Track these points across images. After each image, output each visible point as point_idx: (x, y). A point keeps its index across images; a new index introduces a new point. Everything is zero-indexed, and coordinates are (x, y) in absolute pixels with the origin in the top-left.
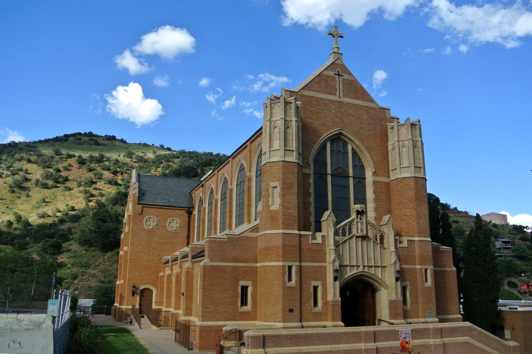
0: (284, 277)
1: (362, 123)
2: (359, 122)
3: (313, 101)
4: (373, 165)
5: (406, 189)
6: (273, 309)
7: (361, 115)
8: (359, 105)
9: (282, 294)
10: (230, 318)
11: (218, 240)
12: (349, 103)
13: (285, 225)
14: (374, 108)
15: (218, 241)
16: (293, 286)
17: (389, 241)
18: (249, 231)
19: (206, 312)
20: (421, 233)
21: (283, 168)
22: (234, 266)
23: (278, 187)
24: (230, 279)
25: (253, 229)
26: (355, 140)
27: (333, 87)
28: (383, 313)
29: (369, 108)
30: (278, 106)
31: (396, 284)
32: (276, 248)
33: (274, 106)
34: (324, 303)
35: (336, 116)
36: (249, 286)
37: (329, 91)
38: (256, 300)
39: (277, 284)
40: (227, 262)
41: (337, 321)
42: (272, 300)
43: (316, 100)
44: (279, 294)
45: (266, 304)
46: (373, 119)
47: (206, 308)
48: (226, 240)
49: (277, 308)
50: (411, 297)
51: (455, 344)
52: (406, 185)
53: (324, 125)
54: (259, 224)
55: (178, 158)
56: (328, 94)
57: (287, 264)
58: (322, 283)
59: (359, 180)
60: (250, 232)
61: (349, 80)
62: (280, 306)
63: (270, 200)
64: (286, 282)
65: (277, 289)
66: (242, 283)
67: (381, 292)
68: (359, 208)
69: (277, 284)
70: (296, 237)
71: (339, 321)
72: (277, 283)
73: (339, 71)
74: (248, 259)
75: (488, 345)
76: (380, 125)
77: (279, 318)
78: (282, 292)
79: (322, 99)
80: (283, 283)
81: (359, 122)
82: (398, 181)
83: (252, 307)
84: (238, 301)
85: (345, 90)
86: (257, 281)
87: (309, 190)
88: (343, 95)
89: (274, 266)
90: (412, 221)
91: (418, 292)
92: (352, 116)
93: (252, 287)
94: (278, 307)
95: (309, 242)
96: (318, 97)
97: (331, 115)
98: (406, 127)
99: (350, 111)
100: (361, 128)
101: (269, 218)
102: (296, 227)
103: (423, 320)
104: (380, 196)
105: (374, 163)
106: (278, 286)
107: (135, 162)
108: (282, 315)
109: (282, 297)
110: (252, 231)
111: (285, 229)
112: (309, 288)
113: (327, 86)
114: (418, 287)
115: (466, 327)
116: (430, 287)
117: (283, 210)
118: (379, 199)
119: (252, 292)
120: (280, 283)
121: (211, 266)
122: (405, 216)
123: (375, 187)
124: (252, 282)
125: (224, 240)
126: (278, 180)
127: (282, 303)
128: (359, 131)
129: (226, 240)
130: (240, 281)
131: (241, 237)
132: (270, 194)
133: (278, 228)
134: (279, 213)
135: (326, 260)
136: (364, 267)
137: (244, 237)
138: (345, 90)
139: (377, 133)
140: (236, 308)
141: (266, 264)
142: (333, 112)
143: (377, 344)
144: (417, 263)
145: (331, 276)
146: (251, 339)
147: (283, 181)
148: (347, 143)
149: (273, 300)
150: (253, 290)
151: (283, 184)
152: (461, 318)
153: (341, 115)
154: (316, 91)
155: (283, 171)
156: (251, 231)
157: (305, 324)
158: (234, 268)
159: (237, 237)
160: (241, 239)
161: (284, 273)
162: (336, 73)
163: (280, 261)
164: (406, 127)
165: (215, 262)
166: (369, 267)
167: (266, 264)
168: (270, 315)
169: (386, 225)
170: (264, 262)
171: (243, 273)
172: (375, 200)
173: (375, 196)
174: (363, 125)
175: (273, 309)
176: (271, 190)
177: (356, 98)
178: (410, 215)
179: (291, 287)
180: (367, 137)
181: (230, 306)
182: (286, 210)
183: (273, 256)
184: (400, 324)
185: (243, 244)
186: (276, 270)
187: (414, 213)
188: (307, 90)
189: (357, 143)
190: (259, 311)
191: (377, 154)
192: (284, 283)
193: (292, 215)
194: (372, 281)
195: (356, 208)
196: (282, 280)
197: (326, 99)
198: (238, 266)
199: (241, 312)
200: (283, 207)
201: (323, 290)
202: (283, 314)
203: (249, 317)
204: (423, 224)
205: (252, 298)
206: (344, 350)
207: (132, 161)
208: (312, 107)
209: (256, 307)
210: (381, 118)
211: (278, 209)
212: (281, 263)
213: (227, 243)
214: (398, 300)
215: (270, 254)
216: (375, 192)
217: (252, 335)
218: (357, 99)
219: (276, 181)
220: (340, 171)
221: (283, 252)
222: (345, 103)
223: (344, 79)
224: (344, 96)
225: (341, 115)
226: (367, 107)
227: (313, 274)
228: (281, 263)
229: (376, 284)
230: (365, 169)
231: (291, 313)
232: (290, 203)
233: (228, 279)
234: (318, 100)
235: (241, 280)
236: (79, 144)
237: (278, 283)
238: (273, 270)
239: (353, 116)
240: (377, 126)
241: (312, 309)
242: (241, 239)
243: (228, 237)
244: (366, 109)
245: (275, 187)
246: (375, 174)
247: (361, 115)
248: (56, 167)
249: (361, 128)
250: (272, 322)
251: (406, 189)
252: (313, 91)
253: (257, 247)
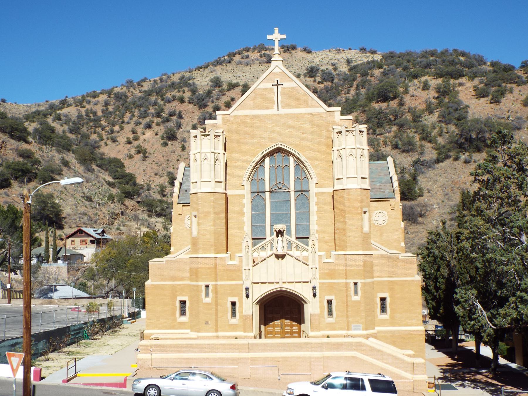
1: (303, 133)
5: (340, 202)
7: (302, 124)
11: (157, 263)
12: (289, 114)
16: (209, 302)
19: (150, 323)
20: (351, 247)
22: (172, 285)
27: (271, 100)
35: (274, 131)
37: (266, 106)
41: (248, 333)
43: (250, 118)
46: (317, 126)
47: (149, 319)
51: (265, 359)
52: (339, 197)
53: (260, 143)
55: (380, 67)
56: (264, 109)
58: (239, 299)
60: (185, 254)
61: (290, 88)
68: (281, 228)
73: (277, 81)
75: (382, 360)
76: (326, 132)
79: (258, 116)
81: (301, 132)
85: (284, 100)
87: (243, 211)
88: (282, 106)
92: (292, 127)
97: (268, 131)
100: (303, 139)
103: (344, 332)
104: (324, 208)
107: (319, 83)
113: (264, 100)
115: (355, 343)
116: (359, 301)
118: (322, 211)
121: (152, 285)
129: (164, 262)
138: (284, 100)
139: (322, 141)
140: (175, 318)
142: (270, 128)
143: (250, 354)
152: (422, 330)
153: (279, 128)
154: (251, 109)
157: (220, 334)
173: (318, 208)
174: (305, 135)
180: (309, 147)
188: (241, 109)
191: (322, 164)
195: (278, 228)
197: (262, 115)
198: (176, 284)
204: (355, 237)
206: (220, 358)
207: (315, 81)
208: (247, 127)
210: (328, 123)
218: (299, 108)
220: (280, 186)
224: (283, 107)
225: (279, 128)
226: (311, 114)
232: (206, 230)
234: (253, 118)
235: (178, 296)
236: (247, 64)
239: (293, 127)
241: (228, 321)
244: (310, 116)
247: (302, 124)
248: (217, 104)
249: (303, 139)
251: (340, 202)
252: (247, 109)
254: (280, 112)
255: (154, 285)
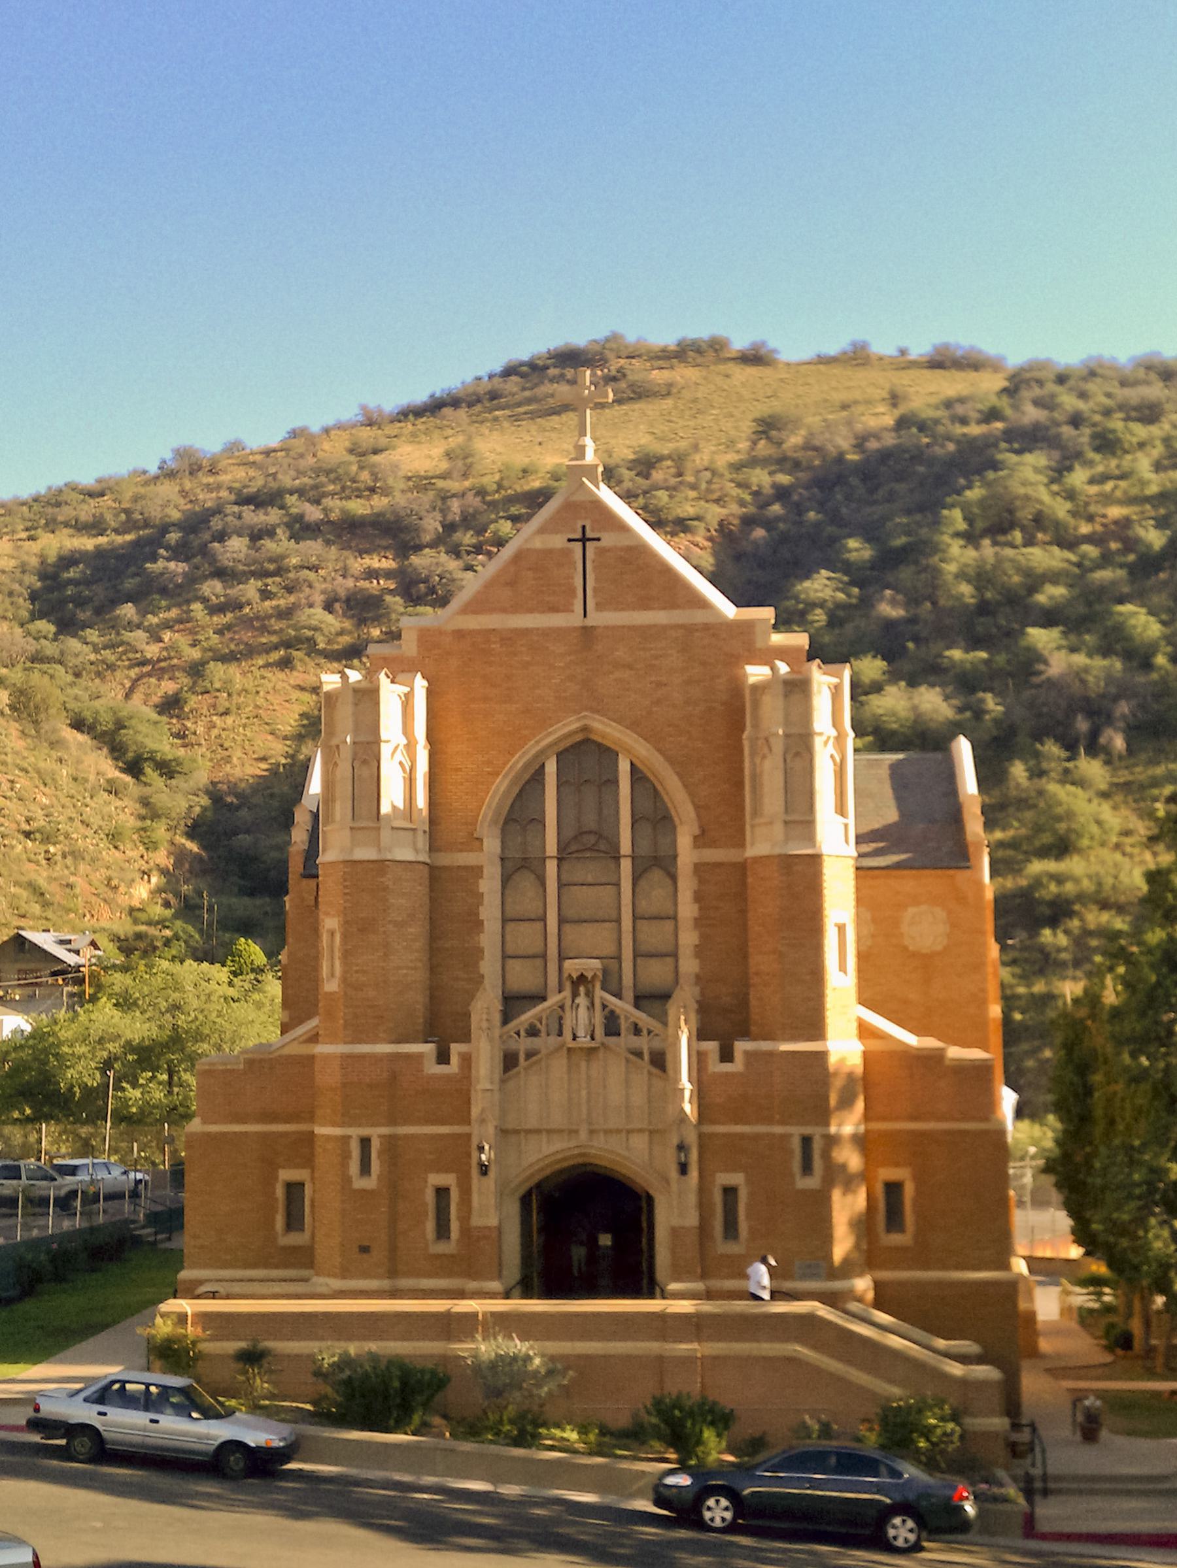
0: (344, 1165)
3: (495, 643)
7: (656, 657)
8: (655, 626)
14: (706, 627)
21: (345, 880)
29: (689, 629)
46: (704, 664)
50: (748, 1217)
66: (286, 1175)
73: (584, 527)
79: (525, 632)
100: (658, 702)
105: (697, 807)
111: (352, 1042)
123: (701, 881)
136: (592, 1132)
154: (504, 610)
158: (264, 1136)
162: (588, 529)
166: (607, 1132)
172: (698, 922)
177: (645, 604)
184: (291, 1280)
197: (538, 629)
216: (698, 897)
223: (601, 552)
224: (599, 607)
230: (674, 828)
231: (365, 1256)
239: (630, 667)
246: (701, 840)
247: (656, 657)
249: (658, 702)
254: (591, 621)
255: (208, 1134)
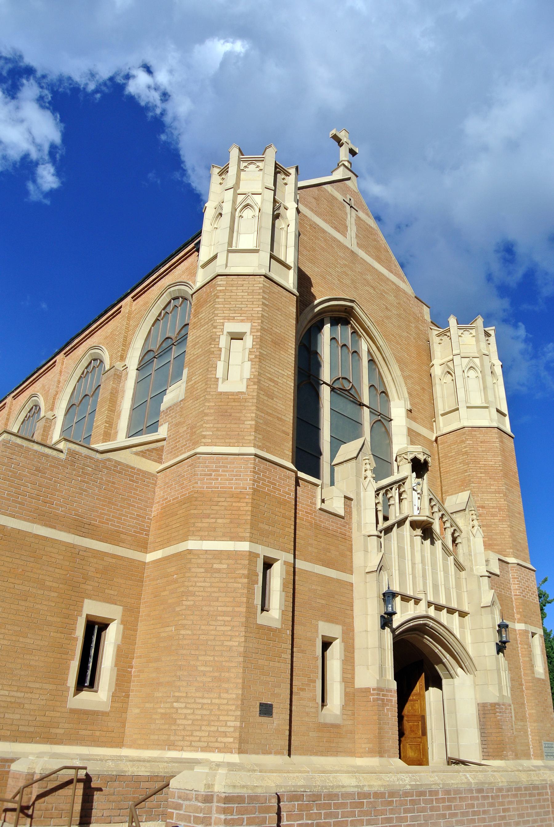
2: (384, 304)
4: (406, 395)
5: (483, 451)
6: (205, 701)
7: (386, 293)
9: (242, 649)
10: (31, 729)
13: (260, 436)
15: (36, 451)
17: (470, 551)
18: (134, 449)
21: (264, 292)
22: (73, 546)
23: (248, 333)
24: (55, 585)
25: (148, 450)
26: (376, 334)
28: (463, 742)
30: (258, 169)
31: (497, 660)
32: (232, 497)
33: (246, 167)
34: (346, 694)
36: (114, 620)
38: (131, 672)
39: (225, 614)
40: (54, 528)
42: (203, 668)
44: (231, 647)
45: (178, 683)
48: (62, 456)
49: (220, 697)
54: (164, 439)
57: (263, 551)
58: (343, 632)
59: (379, 418)
60: (137, 454)
62: (235, 692)
63: (220, 366)
64: (256, 608)
65: (223, 628)
67: (456, 680)
68: (419, 453)
69: (225, 614)
70: (289, 477)
71: (394, 757)
72: (224, 609)
74: (122, 533)
77: (225, 734)
78: (243, 639)
80: (248, 612)
81: (384, 304)
82: (464, 433)
83: (115, 697)
84: (68, 668)
86: (138, 608)
89: (219, 555)
90: (500, 521)
91: (523, 691)
93: (122, 626)
94: (224, 695)
95: (315, 504)
96: (314, 222)
98: (474, 334)
99: (369, 277)
101: (212, 411)
102: (287, 452)
106: (229, 619)
108: (238, 724)
109: (241, 659)
110: (143, 454)
112: (313, 642)
114: (523, 677)
117: (258, 396)
119: (119, 642)
120: (237, 609)
122: (483, 507)
124: (124, 611)
125: (55, 453)
126: (250, 319)
127: (240, 681)
128: (383, 321)
130: (87, 601)
131: (109, 460)
132: (220, 350)
133: (240, 441)
134: (246, 400)
135: (352, 567)
137: (118, 463)
140: (61, 696)
141: (192, 545)
144: (517, 616)
145: (370, 612)
146: (225, 811)
147: (262, 322)
148: (360, 337)
149: (208, 669)
150: (125, 637)
151: (263, 329)
155: (264, 298)
156: (142, 452)
159: (99, 456)
160: (107, 468)
161: (251, 575)
163: (242, 539)
164: (474, 334)
165: (14, 517)
167: (192, 545)
168: (193, 724)
169: (462, 513)
170: (185, 539)
171: (99, 575)
174: (389, 313)
175: (205, 701)
176: (223, 341)
178: (493, 507)
179: (270, 629)
181: (37, 685)
182: (266, 398)
183: (220, 521)
185: (114, 483)
186: (225, 566)
187: (503, 502)
189: (381, 342)
190: (137, 711)
192: (250, 614)
193: (280, 416)
194: (438, 649)
195: (411, 452)
196: (245, 600)
197: (329, 234)
198: (86, 550)
199: (73, 711)
200: (260, 389)
201: (345, 656)
202: (241, 722)
203: (98, 733)
205: (116, 665)
209: (128, 696)
211: (244, 389)
212: (244, 546)
213: (63, 466)
214: (503, 705)
215: (208, 516)
217: (230, 791)
219: (242, 321)
221: (252, 511)
222: (361, 258)
227: (323, 602)
228: (244, 546)
229: (447, 658)
231: (265, 719)
233: (48, 583)
237: (229, 609)
238: (215, 566)
240: (411, 326)
242: (107, 468)
243: (69, 449)
244: (394, 287)
245: (237, 337)
247: (386, 293)
250: (196, 749)
251: (483, 451)
253: (152, 503)
